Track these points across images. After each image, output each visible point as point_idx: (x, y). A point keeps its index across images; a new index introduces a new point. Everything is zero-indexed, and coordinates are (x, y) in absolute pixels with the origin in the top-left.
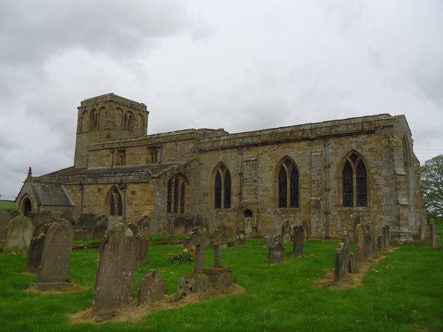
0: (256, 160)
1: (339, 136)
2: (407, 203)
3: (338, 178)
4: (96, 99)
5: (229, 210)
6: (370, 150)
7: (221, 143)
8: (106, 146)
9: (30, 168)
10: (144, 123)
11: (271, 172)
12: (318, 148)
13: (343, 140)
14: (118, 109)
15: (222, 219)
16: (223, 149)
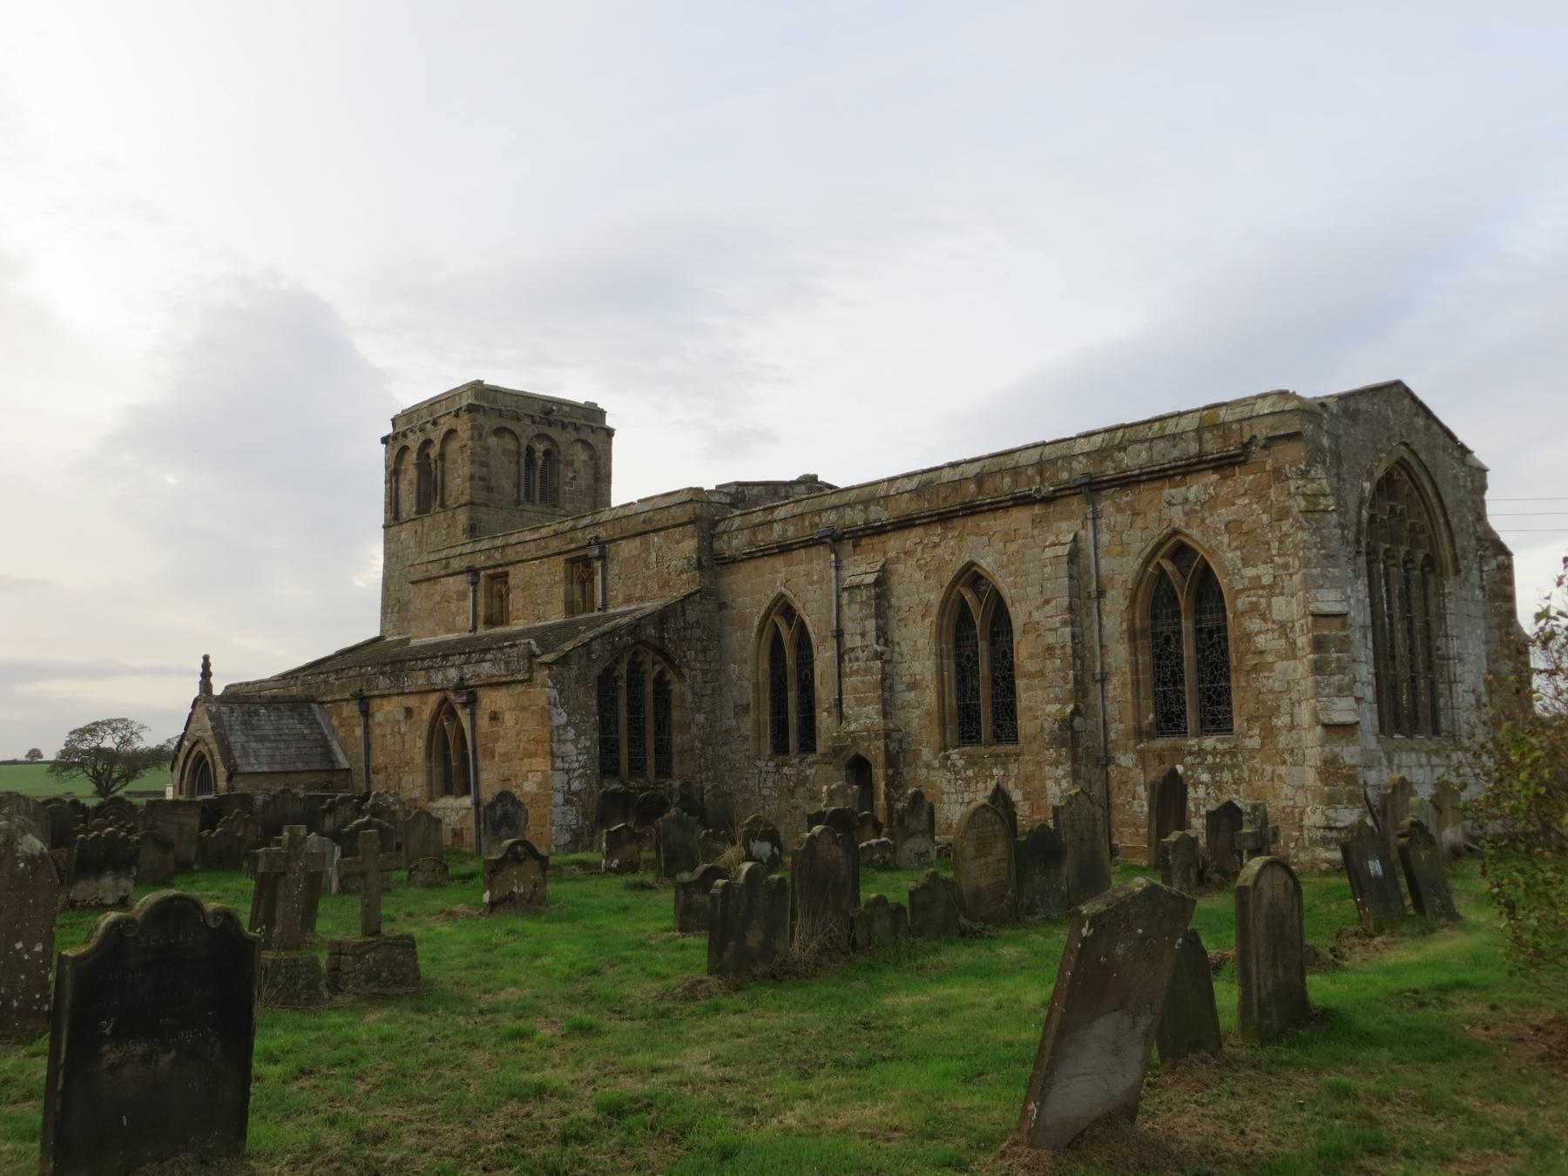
0: (877, 583)
1: (1126, 482)
2: (1349, 718)
3: (1133, 634)
4: (433, 403)
5: (811, 758)
6: (1232, 527)
7: (777, 527)
8: (456, 564)
9: (206, 658)
10: (596, 466)
11: (927, 621)
12: (1065, 528)
13: (1145, 493)
14: (500, 432)
15: (792, 793)
16: (784, 549)
